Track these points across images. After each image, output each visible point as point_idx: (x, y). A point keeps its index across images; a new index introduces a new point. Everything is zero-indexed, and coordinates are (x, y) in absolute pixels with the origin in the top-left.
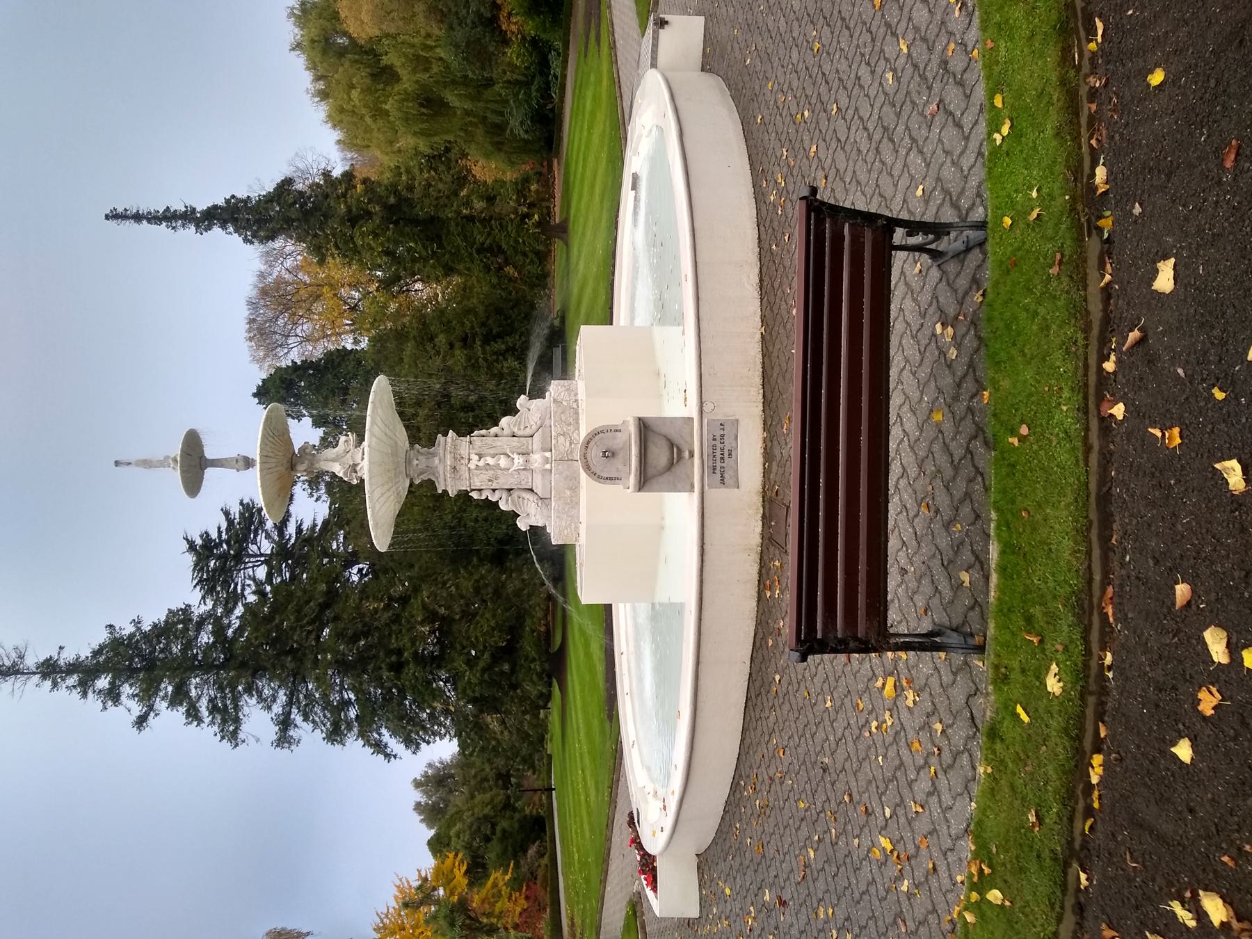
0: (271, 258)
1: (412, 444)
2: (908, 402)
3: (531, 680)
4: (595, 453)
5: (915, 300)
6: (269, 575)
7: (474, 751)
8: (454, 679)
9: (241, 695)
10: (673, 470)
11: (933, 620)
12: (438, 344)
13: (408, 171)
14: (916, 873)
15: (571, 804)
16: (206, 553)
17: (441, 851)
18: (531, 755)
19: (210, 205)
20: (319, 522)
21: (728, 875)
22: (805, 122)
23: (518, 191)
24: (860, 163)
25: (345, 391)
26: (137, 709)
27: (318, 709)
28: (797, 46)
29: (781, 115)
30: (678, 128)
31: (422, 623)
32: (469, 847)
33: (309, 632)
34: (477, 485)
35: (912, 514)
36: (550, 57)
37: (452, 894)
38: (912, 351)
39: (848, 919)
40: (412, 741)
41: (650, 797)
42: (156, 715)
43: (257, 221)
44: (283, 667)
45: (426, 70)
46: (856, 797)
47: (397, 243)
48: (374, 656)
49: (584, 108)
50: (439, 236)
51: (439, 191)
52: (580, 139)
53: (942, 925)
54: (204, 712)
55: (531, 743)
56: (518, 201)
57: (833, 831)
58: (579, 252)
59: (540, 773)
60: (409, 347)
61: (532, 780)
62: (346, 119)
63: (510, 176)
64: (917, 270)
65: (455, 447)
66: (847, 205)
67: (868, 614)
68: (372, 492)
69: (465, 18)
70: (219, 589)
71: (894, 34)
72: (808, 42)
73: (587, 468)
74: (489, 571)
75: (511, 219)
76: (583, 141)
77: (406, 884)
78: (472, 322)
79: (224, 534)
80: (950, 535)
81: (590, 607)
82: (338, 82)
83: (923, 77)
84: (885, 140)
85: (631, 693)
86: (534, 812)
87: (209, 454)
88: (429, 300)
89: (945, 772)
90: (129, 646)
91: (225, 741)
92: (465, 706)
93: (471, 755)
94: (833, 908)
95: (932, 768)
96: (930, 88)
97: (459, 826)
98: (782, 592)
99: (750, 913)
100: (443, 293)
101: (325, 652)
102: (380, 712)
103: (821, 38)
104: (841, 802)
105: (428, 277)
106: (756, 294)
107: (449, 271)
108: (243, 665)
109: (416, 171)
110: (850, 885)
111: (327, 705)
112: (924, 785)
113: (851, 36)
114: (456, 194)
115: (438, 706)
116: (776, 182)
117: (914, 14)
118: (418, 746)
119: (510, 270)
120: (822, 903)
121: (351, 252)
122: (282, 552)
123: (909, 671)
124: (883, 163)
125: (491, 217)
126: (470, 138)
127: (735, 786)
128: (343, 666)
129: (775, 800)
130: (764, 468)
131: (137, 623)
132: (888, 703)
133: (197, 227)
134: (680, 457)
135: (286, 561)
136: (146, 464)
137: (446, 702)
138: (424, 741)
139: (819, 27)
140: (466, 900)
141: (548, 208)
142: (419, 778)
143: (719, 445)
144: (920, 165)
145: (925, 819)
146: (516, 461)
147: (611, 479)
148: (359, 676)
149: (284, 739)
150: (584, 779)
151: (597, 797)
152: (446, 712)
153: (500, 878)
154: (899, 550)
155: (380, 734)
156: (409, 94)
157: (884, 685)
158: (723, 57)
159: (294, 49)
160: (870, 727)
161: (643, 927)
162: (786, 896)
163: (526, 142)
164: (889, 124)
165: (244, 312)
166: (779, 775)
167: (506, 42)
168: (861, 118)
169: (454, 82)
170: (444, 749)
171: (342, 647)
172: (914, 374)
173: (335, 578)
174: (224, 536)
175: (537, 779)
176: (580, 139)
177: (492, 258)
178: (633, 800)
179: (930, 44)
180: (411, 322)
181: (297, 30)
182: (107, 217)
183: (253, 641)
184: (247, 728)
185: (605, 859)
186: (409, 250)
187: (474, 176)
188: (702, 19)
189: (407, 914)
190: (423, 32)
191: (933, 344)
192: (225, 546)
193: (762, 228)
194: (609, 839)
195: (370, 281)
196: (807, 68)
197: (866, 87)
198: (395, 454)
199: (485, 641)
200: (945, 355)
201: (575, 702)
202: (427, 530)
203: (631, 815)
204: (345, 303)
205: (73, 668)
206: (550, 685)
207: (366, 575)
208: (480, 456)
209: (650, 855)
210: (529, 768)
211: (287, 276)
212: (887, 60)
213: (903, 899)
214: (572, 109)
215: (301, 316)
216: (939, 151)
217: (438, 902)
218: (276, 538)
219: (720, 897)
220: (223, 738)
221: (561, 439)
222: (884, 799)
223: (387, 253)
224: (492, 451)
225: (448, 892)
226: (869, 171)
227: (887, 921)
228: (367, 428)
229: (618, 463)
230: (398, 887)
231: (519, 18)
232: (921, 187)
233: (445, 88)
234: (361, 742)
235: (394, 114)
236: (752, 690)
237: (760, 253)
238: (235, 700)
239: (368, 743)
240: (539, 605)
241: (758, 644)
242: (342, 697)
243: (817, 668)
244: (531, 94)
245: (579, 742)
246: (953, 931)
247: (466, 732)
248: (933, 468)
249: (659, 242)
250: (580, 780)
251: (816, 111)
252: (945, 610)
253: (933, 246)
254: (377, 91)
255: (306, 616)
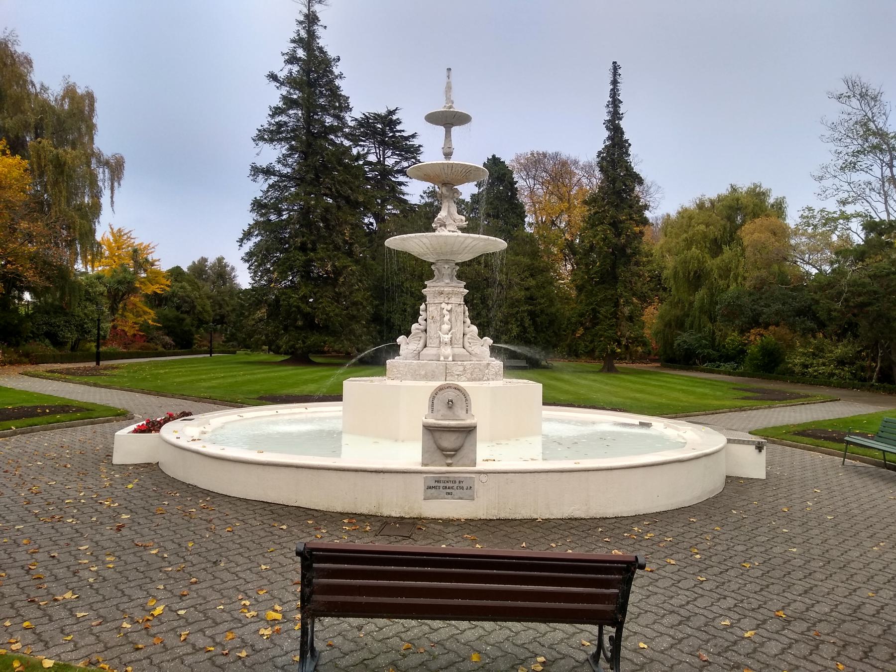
0: (587, 169)
1: (457, 264)
2: (486, 633)
3: (290, 341)
4: (451, 394)
5: (562, 640)
6: (370, 163)
7: (241, 299)
8: (293, 287)
9: (288, 143)
10: (438, 450)
11: (323, 651)
12: (529, 280)
13: (649, 262)
14: (135, 634)
15: (200, 368)
16: (387, 122)
17: (171, 276)
18: (236, 339)
19: (624, 130)
20: (406, 197)
21: (142, 487)
22: (692, 555)
23: (637, 338)
24: (663, 598)
25: (497, 217)
26: (282, 75)
27: (277, 194)
28: (747, 550)
29: (696, 536)
30: (685, 459)
31: (333, 265)
32: (174, 294)
33: (330, 189)
34: (430, 309)
35: (403, 635)
36: (733, 363)
37: (141, 283)
38: (524, 637)
39: (105, 579)
40: (251, 257)
41: (202, 429)
42: (277, 87)
43: (613, 160)
44: (307, 172)
45: (720, 276)
46: (194, 587)
47: (599, 254)
48: (312, 233)
49: (697, 387)
50: (603, 282)
51: (635, 283)
52: (675, 383)
53: (96, 655)
54: (278, 119)
55: (245, 339)
56: (630, 338)
57: (170, 569)
58: (595, 381)
59: (223, 346)
60: (526, 260)
61: (219, 340)
62: (685, 221)
63: (647, 332)
64: (584, 642)
65: (457, 294)
66: (633, 588)
67: (330, 603)
68: (426, 237)
69: (758, 304)
70: (362, 130)
71: (758, 626)
72: (750, 558)
73: (441, 389)
74: (368, 312)
75: (617, 332)
76: (673, 385)
77: (150, 251)
78: (544, 303)
79: (399, 134)
80: (386, 666)
81: (341, 385)
82: (710, 216)
83: (727, 649)
84: (680, 618)
85: (277, 415)
86: (195, 341)
87: (455, 130)
88: (559, 274)
89: (210, 659)
90: (325, 71)
91: (257, 132)
92: (274, 294)
93: (239, 298)
94: (113, 568)
95: (212, 649)
96: (719, 654)
97: (189, 288)
98: (347, 531)
99: (113, 502)
100: (564, 284)
101: (316, 199)
102: (272, 236)
103: (753, 568)
104: (191, 575)
105: (575, 274)
106: (565, 515)
107: (580, 289)
108: (309, 145)
109: (649, 268)
110: (130, 581)
111: (279, 200)
112: (201, 641)
113: (755, 593)
114: (634, 295)
115: (276, 275)
116: (648, 532)
117: (773, 643)
118: (247, 261)
119: (581, 331)
120: (117, 560)
121: (592, 222)
122: (386, 171)
123: (286, 631)
124: (663, 617)
125: (618, 319)
126: (674, 305)
127: (207, 493)
128: (305, 212)
129: (195, 524)
130: (438, 519)
131: (341, 76)
132: (262, 615)
133: (609, 121)
134: (447, 456)
135: (380, 175)
136: (449, 88)
137: (277, 281)
138: (250, 266)
139: (762, 567)
140: (137, 293)
141: (625, 359)
142: (224, 261)
143: (455, 485)
144: (662, 646)
145: (175, 642)
146: (446, 336)
147: (433, 405)
148: (299, 222)
149: (257, 171)
150: (217, 378)
151: (203, 387)
152: (270, 281)
153: (150, 317)
154: (376, 625)
155: (257, 235)
156: (703, 264)
157: (276, 611)
158: (737, 493)
159: (732, 187)
160: (245, 600)
161: (108, 421)
162: (124, 531)
163: (672, 344)
164: (691, 621)
165: (551, 151)
166: (213, 527)
167: (742, 332)
168: (695, 599)
169: (712, 295)
170: (244, 279)
171: (319, 211)
172: (507, 639)
173: (368, 208)
174: (398, 134)
175: (219, 344)
176: (675, 383)
177: (589, 319)
178: (200, 416)
179: (752, 655)
180: (544, 262)
181: (745, 189)
182: (614, 63)
183: (326, 152)
184: (266, 147)
185: (159, 393)
186: (594, 262)
187: (647, 307)
188: (764, 477)
189: (129, 251)
190: (746, 275)
191: (529, 654)
192: (391, 134)
193: (614, 520)
194: (173, 396)
195: (572, 235)
196: (731, 557)
197: (719, 604)
198: (452, 253)
199: (319, 309)
200: (521, 664)
201: (272, 372)
202: (399, 269)
203: (189, 414)
204: (557, 218)
205: (312, 35)
206: (286, 354)
207: (368, 228)
208: (450, 311)
209: (160, 428)
210: (227, 338)
211: (575, 179)
212: (739, 620)
213: (117, 624)
214: (696, 378)
215: (548, 188)
216: (673, 661)
217: (136, 273)
218: (396, 168)
219: (127, 480)
220: (260, 131)
221: (461, 368)
222: (192, 609)
223: (592, 248)
224: (453, 319)
225: (143, 280)
226: (657, 605)
227: (101, 610)
228: (471, 235)
229: (444, 411)
230: (148, 246)
231: (760, 341)
232: (646, 646)
233: (708, 289)
234: (252, 222)
235: (689, 254)
236: (276, 507)
237: (595, 518)
238: (286, 139)
239: (251, 227)
240: (343, 347)
241: (309, 512)
242: (284, 210)
243: (290, 558)
244: (706, 348)
245: (244, 375)
246: (90, 663)
247: (255, 294)
248: (437, 653)
249: (604, 440)
250: (217, 375)
251: (700, 564)
252: (331, 661)
253: (602, 655)
254: (705, 242)
255: (341, 187)
